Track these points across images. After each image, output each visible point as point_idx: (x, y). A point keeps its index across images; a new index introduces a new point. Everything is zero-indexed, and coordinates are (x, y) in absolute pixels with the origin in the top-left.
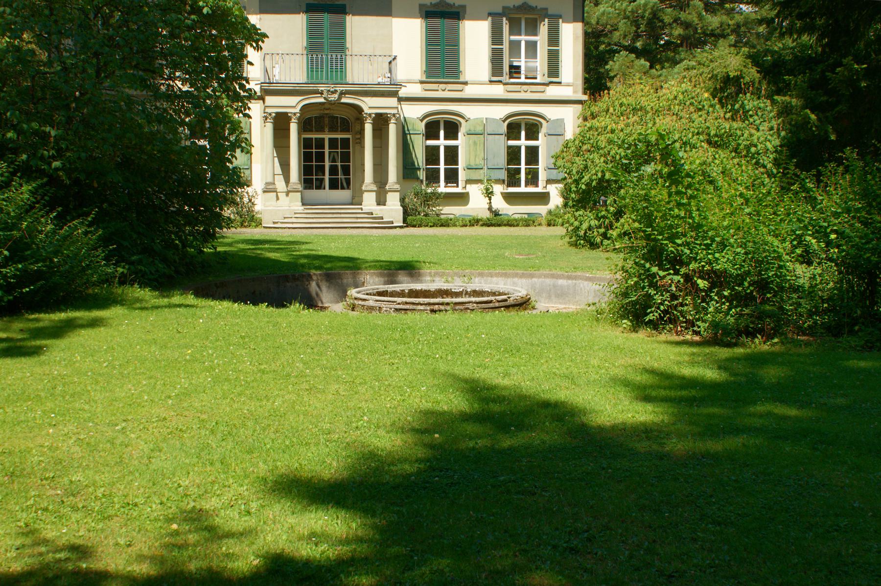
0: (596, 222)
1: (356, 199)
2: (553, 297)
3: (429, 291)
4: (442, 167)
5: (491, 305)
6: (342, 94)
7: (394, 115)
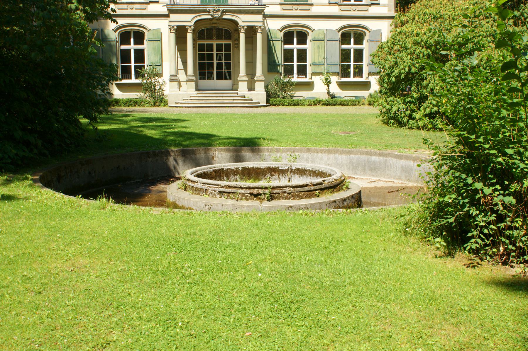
0: (404, 106)
1: (235, 86)
2: (367, 171)
3: (260, 168)
4: (295, 63)
5: (307, 189)
6: (224, 12)
7: (260, 27)
